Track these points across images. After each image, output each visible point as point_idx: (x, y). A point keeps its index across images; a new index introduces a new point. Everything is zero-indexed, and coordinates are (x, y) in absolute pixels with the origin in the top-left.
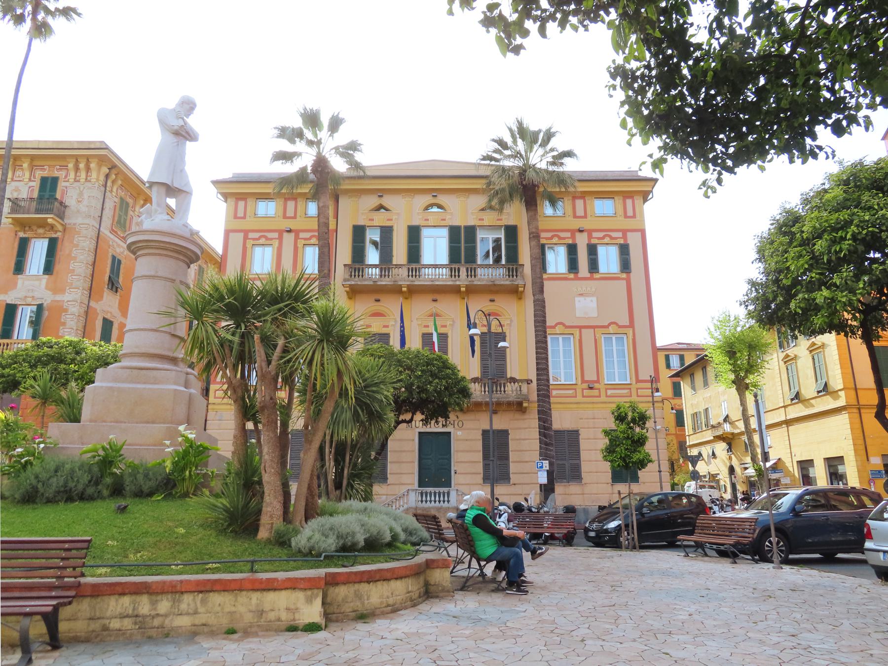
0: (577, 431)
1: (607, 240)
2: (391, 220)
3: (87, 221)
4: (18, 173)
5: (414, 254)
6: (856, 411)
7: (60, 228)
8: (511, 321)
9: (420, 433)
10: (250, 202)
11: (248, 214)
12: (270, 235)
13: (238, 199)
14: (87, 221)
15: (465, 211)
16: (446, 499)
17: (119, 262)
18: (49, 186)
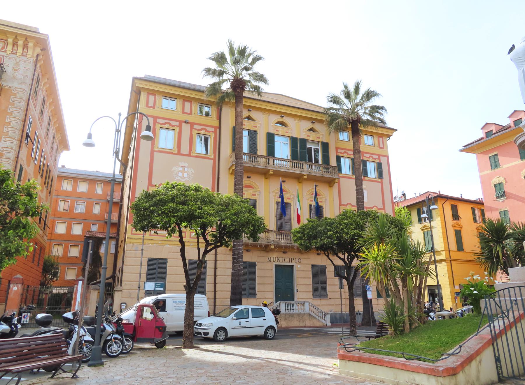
0: (325, 266)
1: (167, 126)
2: (256, 127)
3: (22, 86)
5: (271, 151)
6: (449, 262)
8: (326, 199)
9: (276, 265)
10: (158, 97)
12: (173, 123)
13: (149, 94)
14: (22, 86)
15: (299, 129)
16: (292, 308)
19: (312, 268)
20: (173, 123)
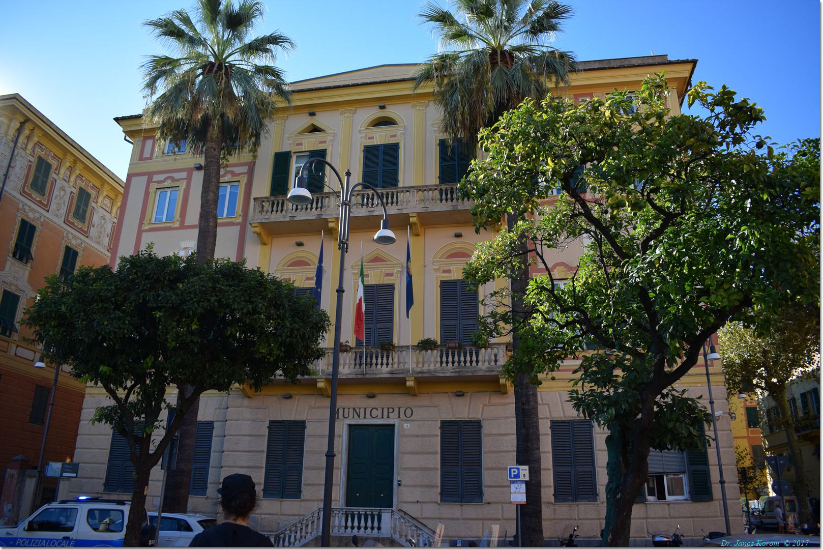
12: (176, 176)
16: (376, 524)
17: (76, 254)
20: (176, 176)
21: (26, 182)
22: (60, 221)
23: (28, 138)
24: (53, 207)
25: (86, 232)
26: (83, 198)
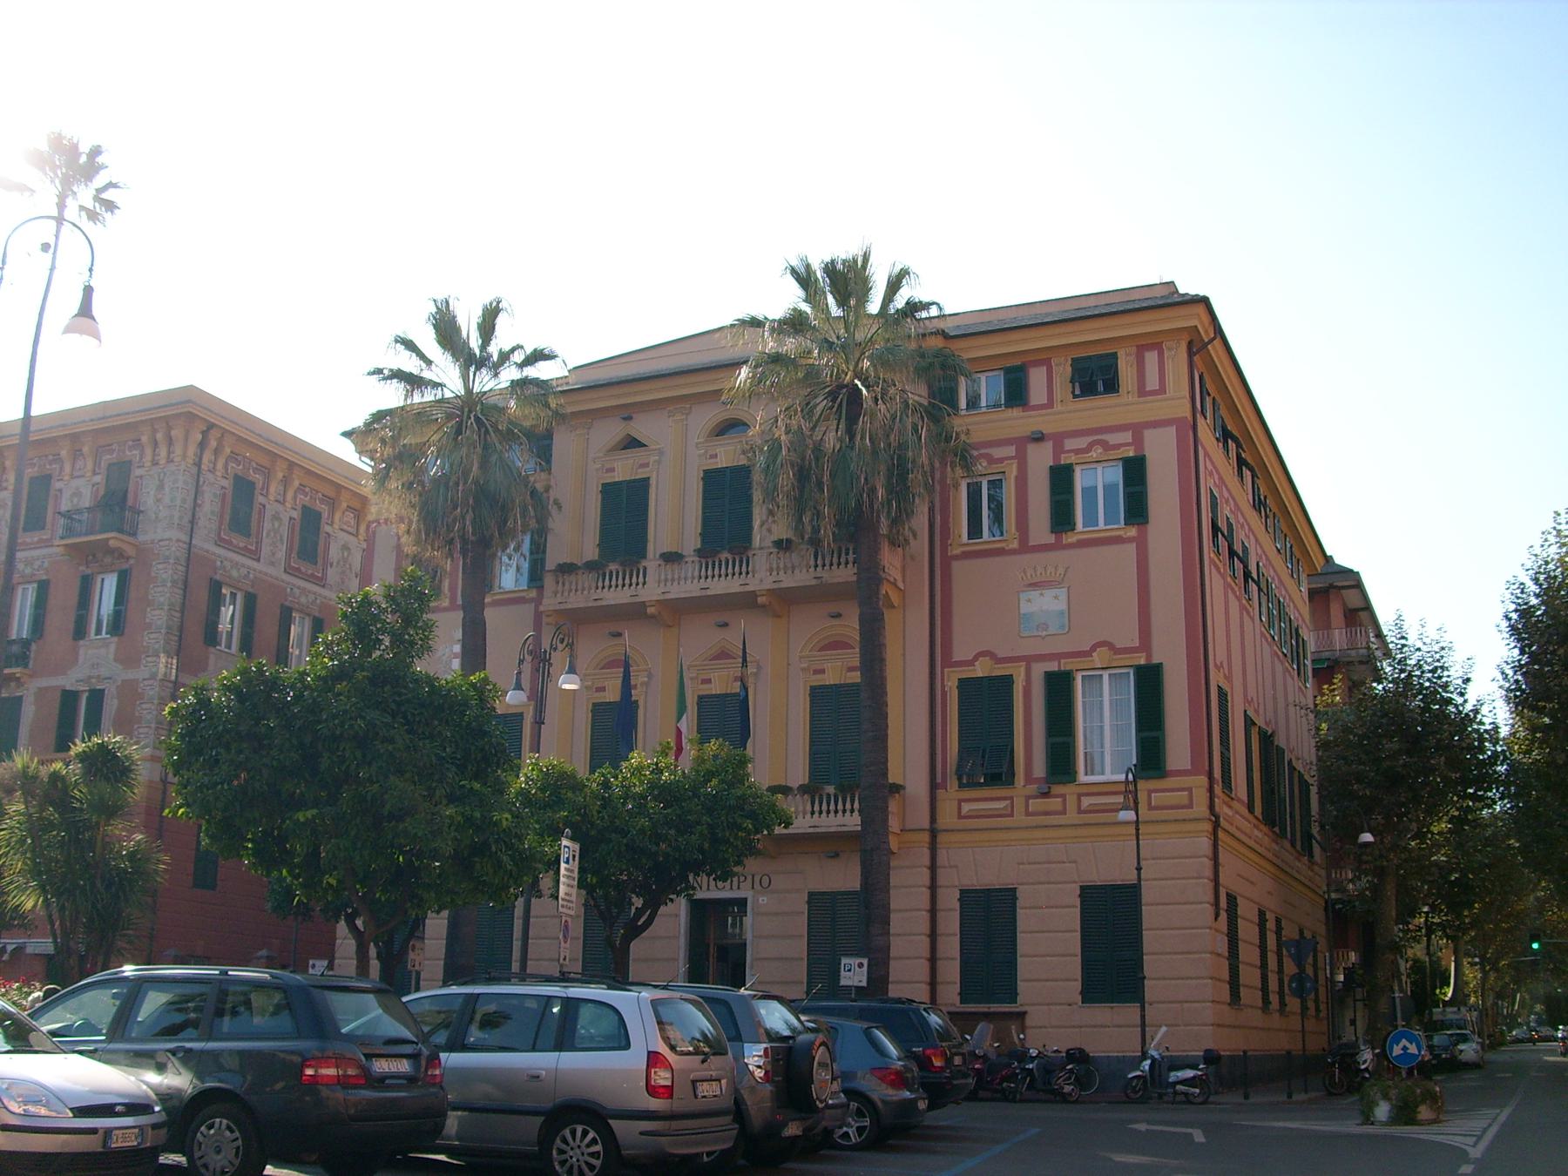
4: (80, 464)
7: (131, 551)
8: (650, 676)
11: (1058, 395)
18: (121, 471)
19: (809, 902)
21: (221, 523)
22: (278, 572)
23: (217, 452)
24: (266, 550)
25: (321, 579)
26: (310, 522)
